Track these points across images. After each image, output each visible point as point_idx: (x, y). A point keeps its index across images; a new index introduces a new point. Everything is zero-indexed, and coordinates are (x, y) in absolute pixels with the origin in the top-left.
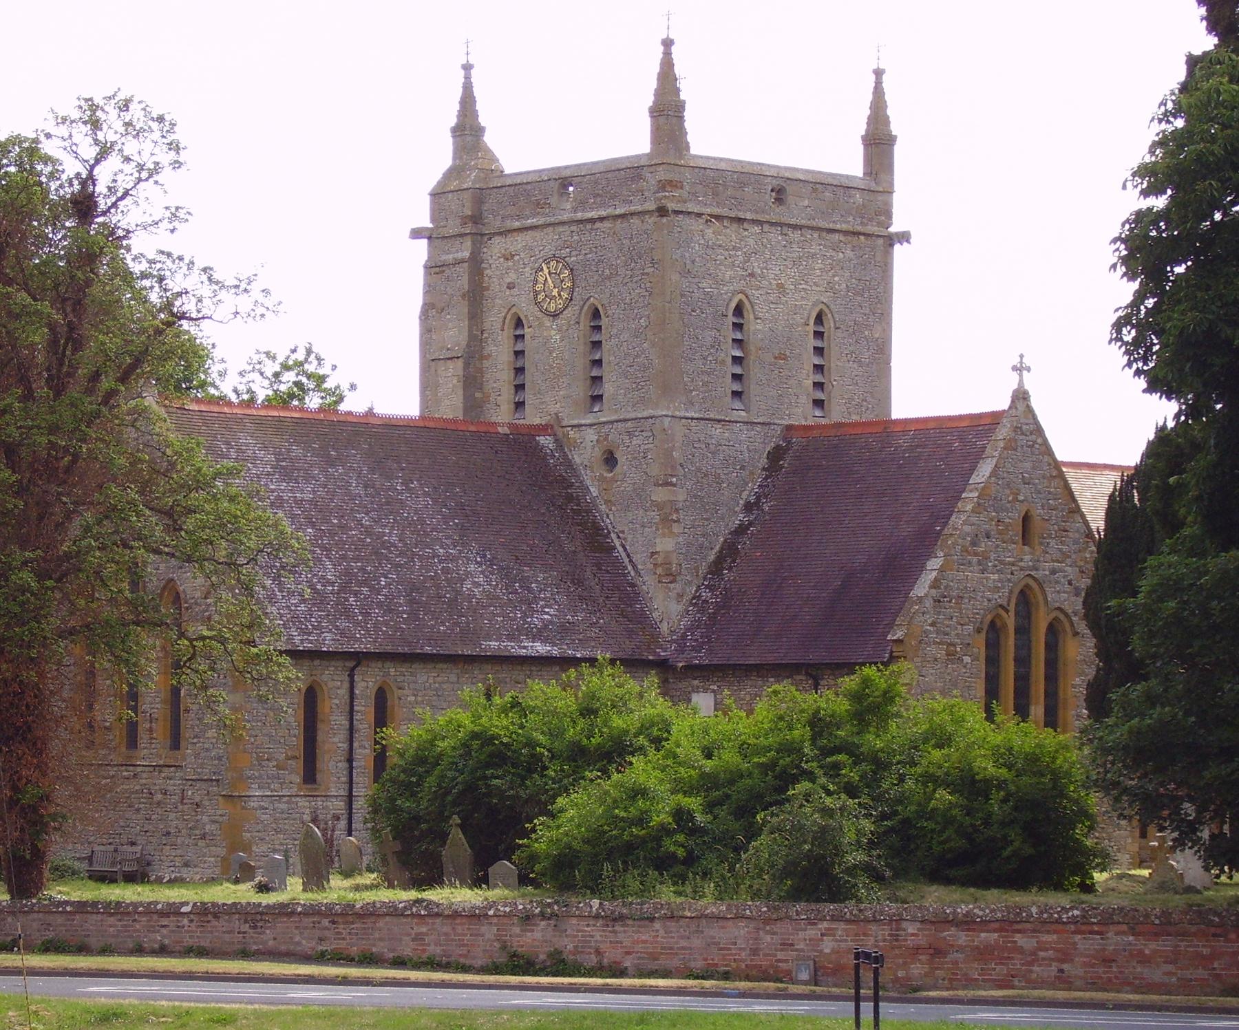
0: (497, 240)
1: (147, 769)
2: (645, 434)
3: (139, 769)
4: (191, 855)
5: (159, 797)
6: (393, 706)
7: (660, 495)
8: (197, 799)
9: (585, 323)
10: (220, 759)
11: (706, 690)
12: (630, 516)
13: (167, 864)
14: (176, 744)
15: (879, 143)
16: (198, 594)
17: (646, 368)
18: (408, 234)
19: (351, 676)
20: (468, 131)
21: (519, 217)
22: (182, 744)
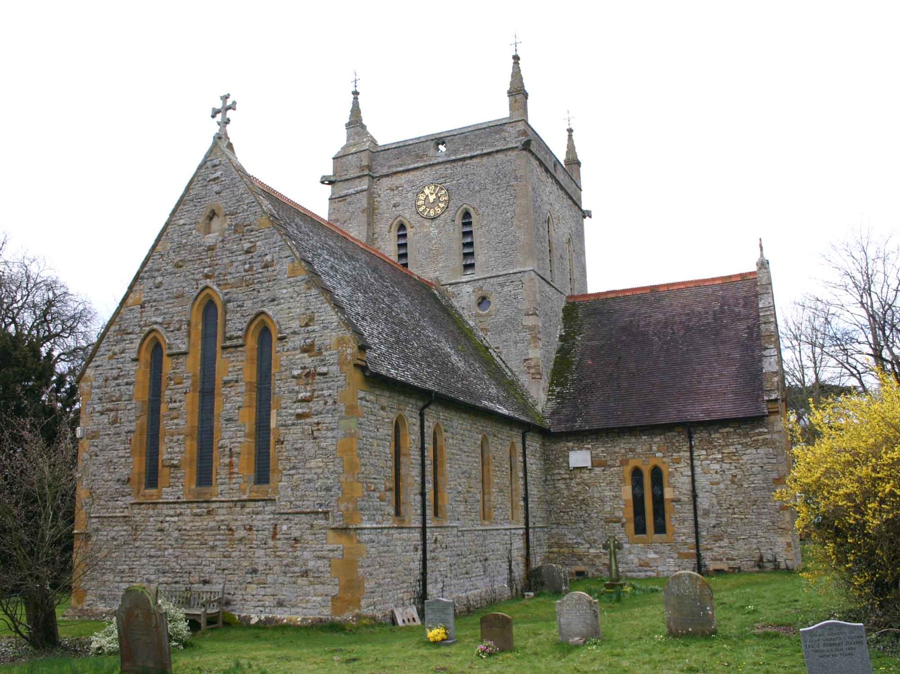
0: (384, 180)
1: (226, 505)
2: (515, 284)
3: (214, 506)
4: (286, 593)
5: (242, 533)
6: (442, 446)
7: (530, 321)
8: (296, 534)
9: (459, 221)
10: (328, 489)
11: (581, 449)
12: (504, 337)
13: (253, 604)
14: (262, 475)
15: (518, 93)
16: (295, 325)
17: (513, 243)
18: (319, 180)
19: (422, 415)
20: (355, 123)
21: (401, 165)
22: (273, 477)
